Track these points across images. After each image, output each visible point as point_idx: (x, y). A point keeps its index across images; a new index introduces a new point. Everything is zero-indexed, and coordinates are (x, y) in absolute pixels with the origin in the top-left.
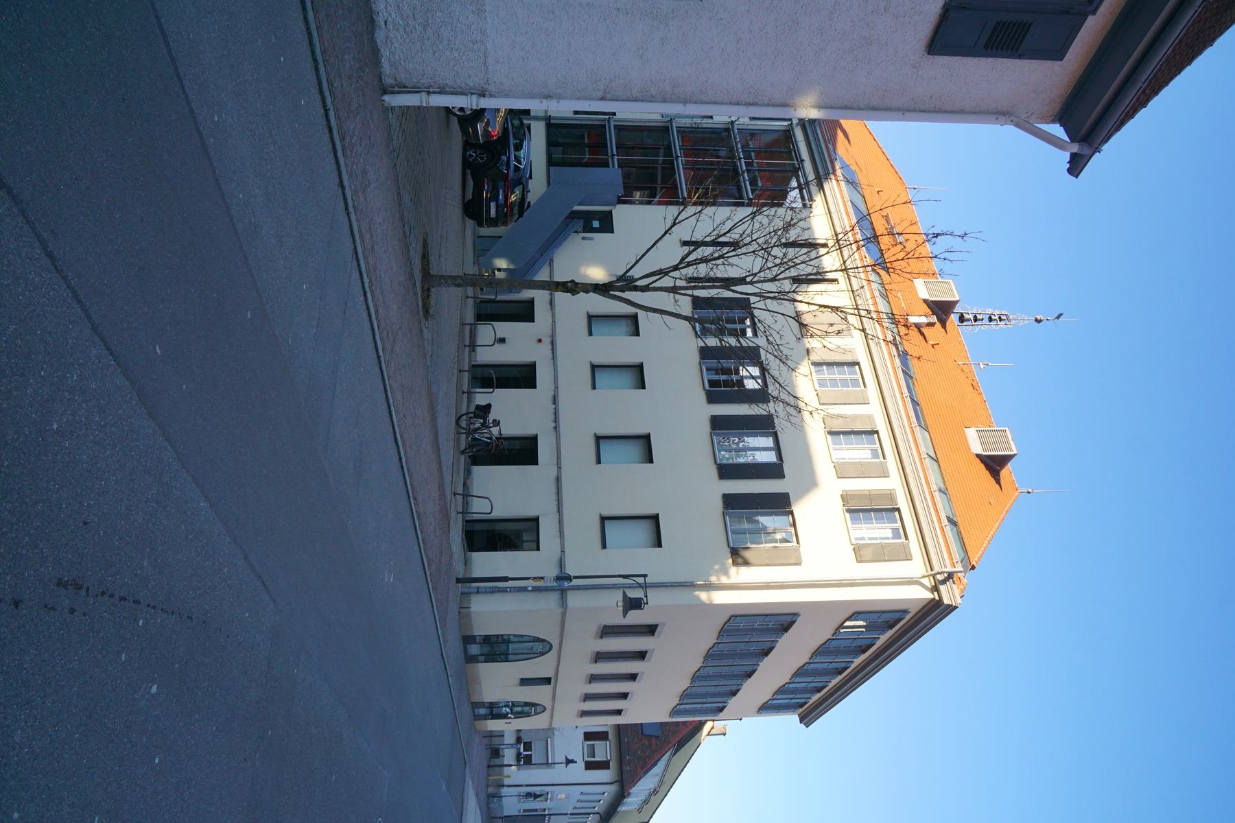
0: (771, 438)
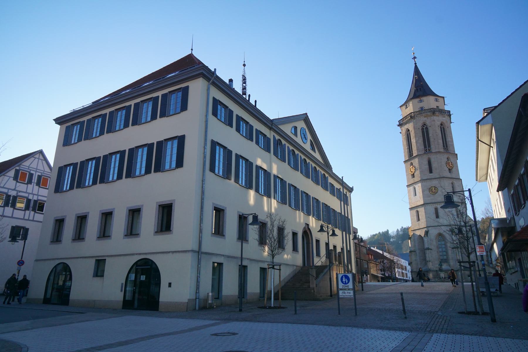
0: (100, 119)
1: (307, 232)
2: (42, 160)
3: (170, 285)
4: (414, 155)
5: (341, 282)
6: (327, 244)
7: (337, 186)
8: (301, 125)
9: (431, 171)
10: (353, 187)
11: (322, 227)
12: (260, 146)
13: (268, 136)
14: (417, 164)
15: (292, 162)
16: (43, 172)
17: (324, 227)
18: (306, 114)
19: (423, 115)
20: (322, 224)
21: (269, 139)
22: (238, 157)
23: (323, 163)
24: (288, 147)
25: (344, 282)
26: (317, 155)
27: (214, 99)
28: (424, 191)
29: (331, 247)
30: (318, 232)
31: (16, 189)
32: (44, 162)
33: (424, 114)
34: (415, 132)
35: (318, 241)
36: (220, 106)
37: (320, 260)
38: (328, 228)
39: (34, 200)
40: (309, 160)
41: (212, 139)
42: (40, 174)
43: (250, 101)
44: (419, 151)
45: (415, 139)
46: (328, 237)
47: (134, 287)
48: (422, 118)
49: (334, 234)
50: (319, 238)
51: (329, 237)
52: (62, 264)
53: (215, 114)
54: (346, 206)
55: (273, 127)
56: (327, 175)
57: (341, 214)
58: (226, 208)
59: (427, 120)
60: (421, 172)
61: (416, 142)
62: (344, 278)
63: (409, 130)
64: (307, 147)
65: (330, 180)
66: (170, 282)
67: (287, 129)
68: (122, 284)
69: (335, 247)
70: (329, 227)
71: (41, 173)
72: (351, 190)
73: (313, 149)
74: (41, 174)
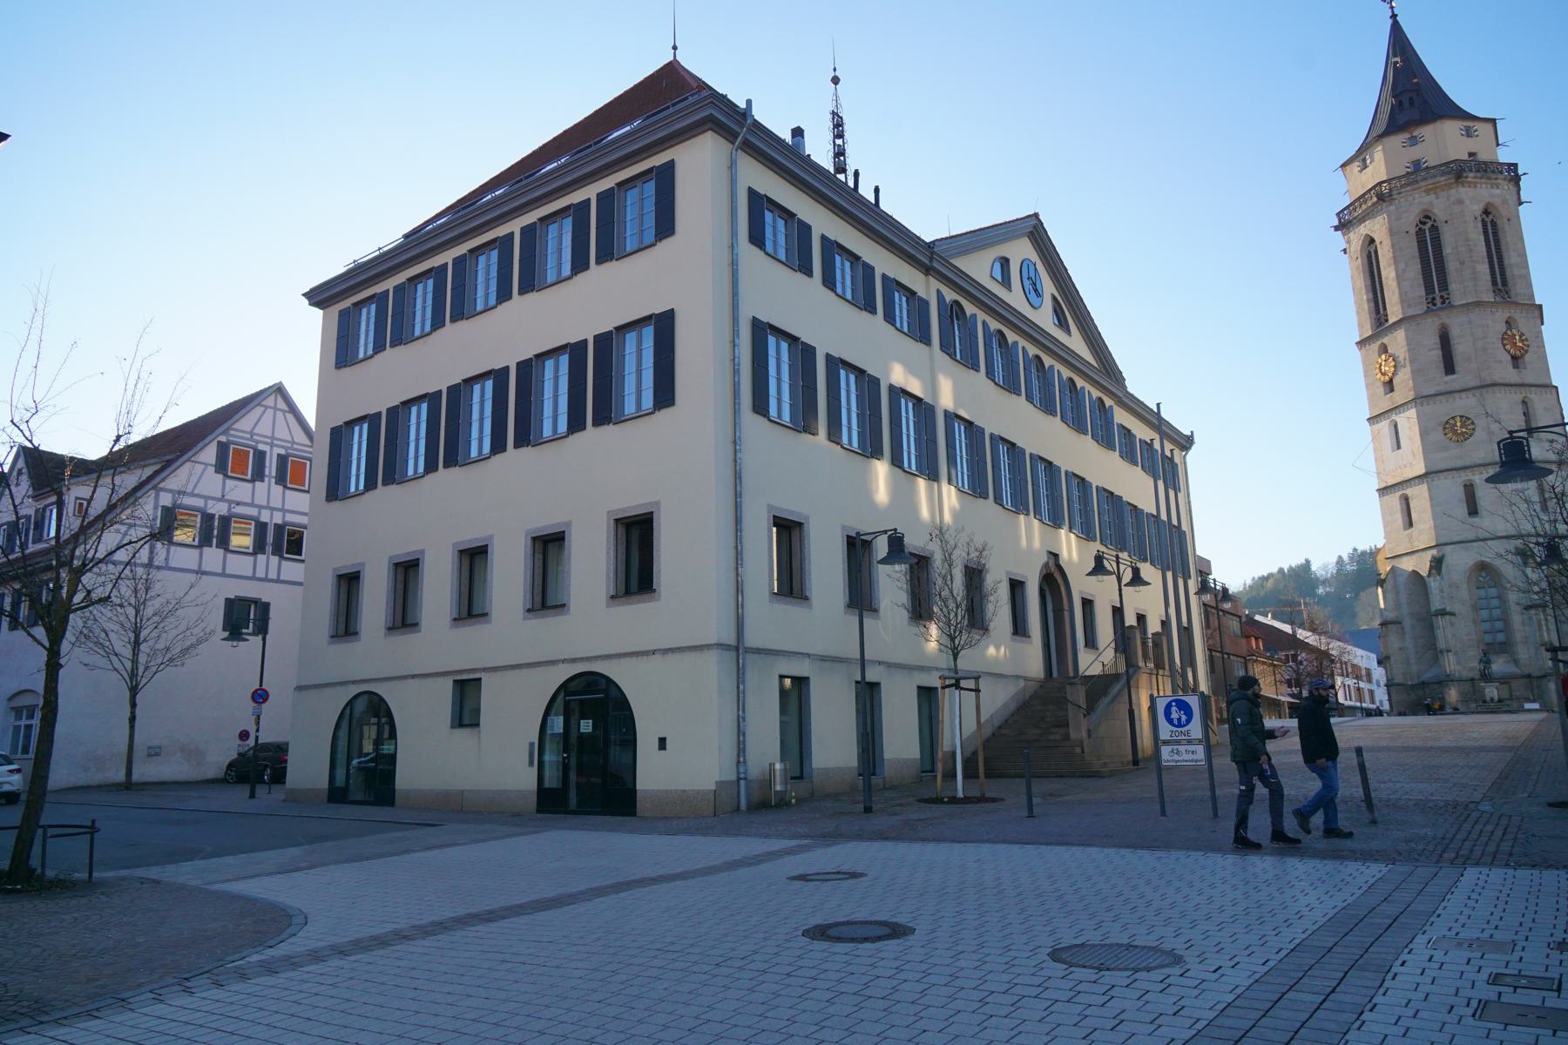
1: (1053, 579)
2: (284, 411)
3: (662, 743)
4: (1392, 320)
6: (1118, 612)
7: (1142, 432)
8: (1021, 251)
9: (1449, 368)
10: (1192, 432)
11: (1099, 559)
13: (921, 293)
14: (1403, 347)
16: (289, 445)
17: (1107, 559)
18: (1036, 215)
19: (1419, 188)
20: (1098, 551)
21: (924, 304)
22: (834, 364)
23: (1096, 365)
24: (984, 323)
25: (1176, 722)
26: (1075, 342)
27: (752, 193)
29: (1130, 620)
32: (290, 417)
33: (1423, 184)
35: (1088, 604)
38: (1118, 563)
39: (275, 524)
42: (282, 452)
43: (861, 191)
45: (1393, 267)
46: (1120, 590)
48: (1417, 196)
49: (1137, 580)
51: (1123, 587)
55: (935, 265)
56: (1108, 402)
57: (1157, 517)
63: (1372, 241)
64: (1044, 318)
68: (532, 745)
69: (1141, 618)
70: (1120, 560)
71: (286, 448)
72: (1186, 443)
73: (1062, 324)
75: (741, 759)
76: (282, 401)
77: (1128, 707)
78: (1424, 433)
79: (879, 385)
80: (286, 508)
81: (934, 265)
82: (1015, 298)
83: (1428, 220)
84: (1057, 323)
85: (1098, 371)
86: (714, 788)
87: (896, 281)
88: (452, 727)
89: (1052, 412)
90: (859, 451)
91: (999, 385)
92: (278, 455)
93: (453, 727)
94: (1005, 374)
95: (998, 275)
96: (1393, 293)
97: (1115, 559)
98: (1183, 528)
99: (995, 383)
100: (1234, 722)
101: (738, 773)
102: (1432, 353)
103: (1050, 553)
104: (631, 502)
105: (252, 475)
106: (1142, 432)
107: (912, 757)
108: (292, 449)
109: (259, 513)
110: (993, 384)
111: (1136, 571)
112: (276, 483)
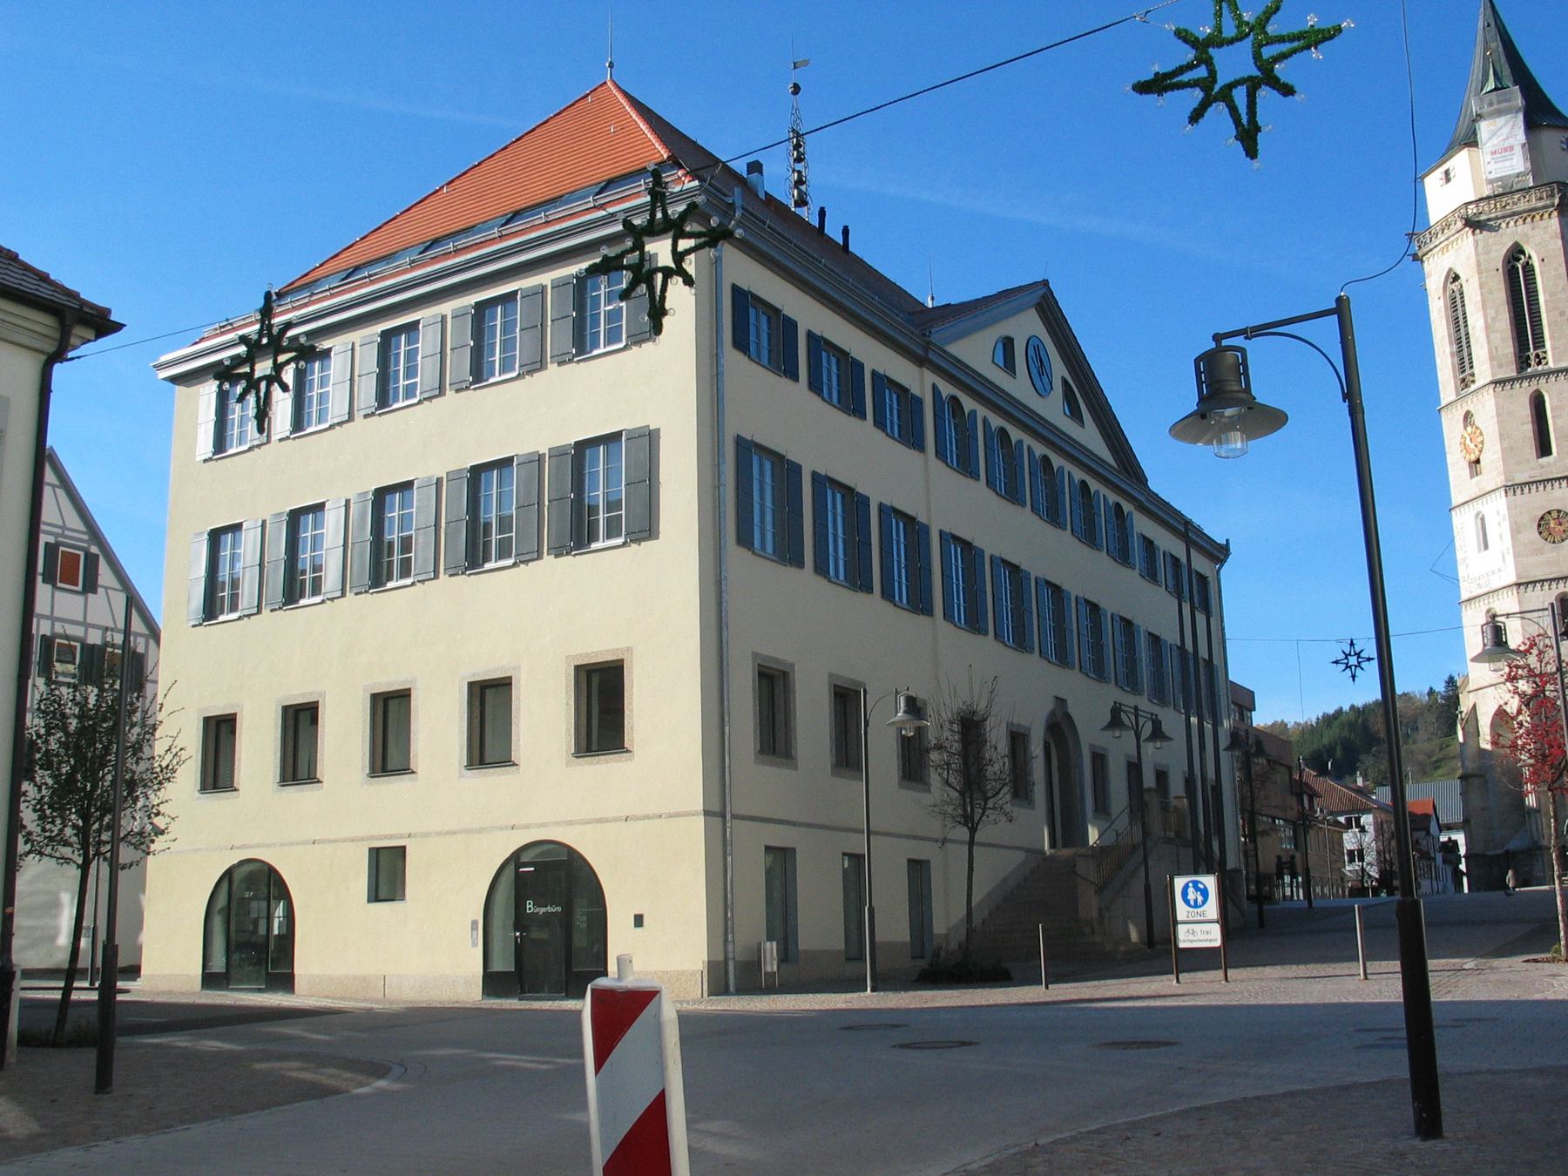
1: (1060, 727)
2: (53, 486)
3: (639, 920)
4: (1480, 381)
5: (1183, 902)
6: (1134, 768)
7: (1168, 543)
8: (1026, 326)
9: (1544, 448)
10: (1227, 541)
11: (1116, 711)
12: (889, 431)
13: (915, 391)
14: (1492, 418)
15: (1000, 475)
16: (59, 531)
17: (1125, 712)
18: (1045, 283)
20: (1115, 703)
21: (918, 402)
22: (820, 481)
23: (1112, 462)
24: (985, 420)
25: (1192, 903)
26: (1089, 436)
27: (736, 290)
28: (1519, 532)
29: (1149, 780)
30: (1105, 728)
31: (100, 631)
32: (61, 493)
34: (1481, 286)
35: (1099, 759)
36: (754, 310)
37: (1109, 827)
38: (1137, 716)
39: (43, 636)
40: (1060, 459)
41: (738, 435)
42: (51, 540)
43: (827, 231)
44: (1500, 366)
45: (1482, 312)
46: (1139, 746)
47: (516, 930)
49: (1158, 734)
50: (1104, 749)
51: (1142, 744)
52: (261, 864)
53: (741, 343)
54: (1201, 619)
55: (931, 356)
56: (1127, 507)
57: (1182, 648)
58: (792, 666)
59: (1530, 233)
60: (1508, 453)
61: (1487, 327)
62: (1191, 890)
63: (1456, 278)
64: (1052, 408)
65: (1142, 525)
66: (639, 913)
67: (976, 351)
68: (475, 923)
69: (1161, 776)
70: (1140, 713)
71: (56, 535)
72: (1219, 553)
73: (1075, 414)
74: (56, 538)
75: (730, 938)
76: (52, 474)
77: (1144, 882)
78: (1516, 531)
79: (869, 506)
80: (89, 621)
81: (930, 356)
82: (1019, 387)
83: (1522, 257)
84: (1068, 413)
85: (1117, 471)
86: (945, 932)
87: (887, 378)
88: (369, 901)
89: (1062, 526)
90: (847, 585)
91: (1000, 496)
92: (47, 544)
93: (369, 901)
94: (1007, 481)
95: (1000, 360)
96: (1482, 347)
97: (1133, 711)
98: (1215, 662)
99: (997, 493)
100: (129, 730)
101: (726, 952)
102: (1525, 427)
103: (1057, 698)
104: (598, 649)
105: (84, 586)
106: (1168, 543)
107: (839, 948)
108: (63, 535)
109: (86, 632)
110: (994, 493)
111: (1157, 724)
112: (44, 581)
